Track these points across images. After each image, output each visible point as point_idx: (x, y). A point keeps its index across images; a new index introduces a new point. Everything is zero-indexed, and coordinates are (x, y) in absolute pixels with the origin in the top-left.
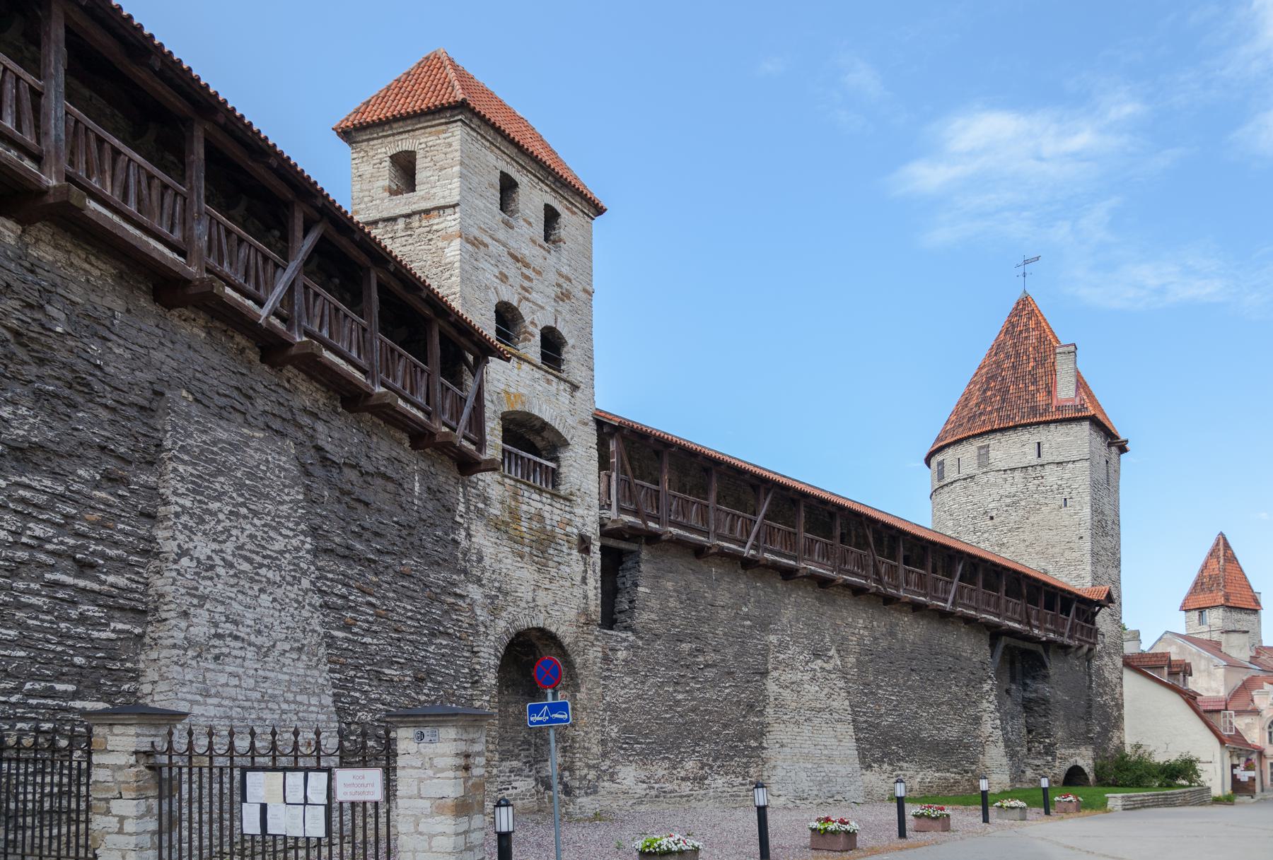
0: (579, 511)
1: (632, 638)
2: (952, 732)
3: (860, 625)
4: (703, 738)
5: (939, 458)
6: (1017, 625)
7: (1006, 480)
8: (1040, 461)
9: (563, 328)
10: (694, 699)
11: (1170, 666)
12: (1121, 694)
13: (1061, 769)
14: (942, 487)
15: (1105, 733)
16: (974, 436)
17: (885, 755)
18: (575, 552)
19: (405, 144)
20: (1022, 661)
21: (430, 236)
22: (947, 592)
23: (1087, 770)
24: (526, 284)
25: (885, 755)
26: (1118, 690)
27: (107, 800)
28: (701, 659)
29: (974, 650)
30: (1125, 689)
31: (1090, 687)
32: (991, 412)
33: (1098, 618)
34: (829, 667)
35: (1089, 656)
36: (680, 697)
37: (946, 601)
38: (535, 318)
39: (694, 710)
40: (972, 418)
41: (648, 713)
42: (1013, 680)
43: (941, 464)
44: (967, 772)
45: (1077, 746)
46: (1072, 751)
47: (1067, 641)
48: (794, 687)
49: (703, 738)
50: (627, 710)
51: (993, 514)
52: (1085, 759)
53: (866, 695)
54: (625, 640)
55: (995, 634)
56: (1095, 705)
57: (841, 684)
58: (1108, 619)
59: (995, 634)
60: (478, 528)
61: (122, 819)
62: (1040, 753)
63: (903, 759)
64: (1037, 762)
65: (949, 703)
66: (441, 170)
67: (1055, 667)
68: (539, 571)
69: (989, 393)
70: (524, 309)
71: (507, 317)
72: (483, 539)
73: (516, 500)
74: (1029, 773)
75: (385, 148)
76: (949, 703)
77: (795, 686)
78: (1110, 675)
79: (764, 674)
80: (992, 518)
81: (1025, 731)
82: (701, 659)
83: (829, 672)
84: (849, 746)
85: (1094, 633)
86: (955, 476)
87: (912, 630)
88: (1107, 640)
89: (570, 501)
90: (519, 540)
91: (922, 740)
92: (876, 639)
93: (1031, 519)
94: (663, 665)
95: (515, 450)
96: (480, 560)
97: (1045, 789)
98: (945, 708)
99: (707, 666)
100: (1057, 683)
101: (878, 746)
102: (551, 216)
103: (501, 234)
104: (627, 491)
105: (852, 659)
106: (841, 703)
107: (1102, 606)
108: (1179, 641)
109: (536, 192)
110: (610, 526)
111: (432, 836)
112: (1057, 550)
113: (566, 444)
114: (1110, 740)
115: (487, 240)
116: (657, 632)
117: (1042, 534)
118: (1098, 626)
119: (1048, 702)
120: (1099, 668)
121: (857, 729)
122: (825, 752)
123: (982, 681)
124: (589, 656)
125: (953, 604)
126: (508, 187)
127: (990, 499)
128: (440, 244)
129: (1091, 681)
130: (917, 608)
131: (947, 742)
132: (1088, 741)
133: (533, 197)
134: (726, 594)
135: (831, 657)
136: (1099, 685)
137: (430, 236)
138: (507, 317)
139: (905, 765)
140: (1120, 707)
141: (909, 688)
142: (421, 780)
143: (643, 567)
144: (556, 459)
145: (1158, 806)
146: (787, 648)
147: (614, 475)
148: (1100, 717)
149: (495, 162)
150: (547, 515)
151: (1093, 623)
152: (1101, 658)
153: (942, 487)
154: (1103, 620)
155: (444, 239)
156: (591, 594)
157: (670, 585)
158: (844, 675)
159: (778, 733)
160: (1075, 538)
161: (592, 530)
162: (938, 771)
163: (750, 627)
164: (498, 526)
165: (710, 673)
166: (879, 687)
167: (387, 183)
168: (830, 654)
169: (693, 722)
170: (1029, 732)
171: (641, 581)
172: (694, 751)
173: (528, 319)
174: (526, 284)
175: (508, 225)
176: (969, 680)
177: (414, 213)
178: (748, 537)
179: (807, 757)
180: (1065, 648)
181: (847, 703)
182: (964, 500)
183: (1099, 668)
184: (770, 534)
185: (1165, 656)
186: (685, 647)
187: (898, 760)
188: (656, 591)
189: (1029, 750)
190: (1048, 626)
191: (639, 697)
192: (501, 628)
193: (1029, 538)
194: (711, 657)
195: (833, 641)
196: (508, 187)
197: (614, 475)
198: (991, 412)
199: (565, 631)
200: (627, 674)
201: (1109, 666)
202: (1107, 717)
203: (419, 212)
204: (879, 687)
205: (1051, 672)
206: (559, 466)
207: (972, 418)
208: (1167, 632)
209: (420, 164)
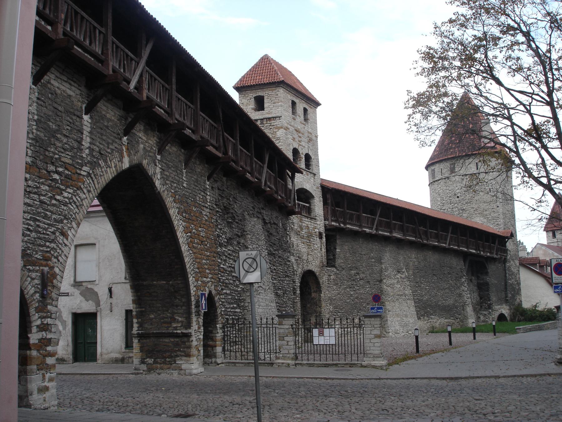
0: (318, 223)
1: (335, 270)
2: (450, 302)
3: (413, 257)
4: (360, 309)
5: (433, 168)
6: (474, 251)
7: (463, 179)
8: (477, 171)
9: (311, 154)
10: (357, 293)
11: (539, 263)
12: (519, 278)
13: (496, 315)
14: (434, 182)
15: (513, 297)
16: (448, 159)
17: (425, 313)
18: (318, 239)
19: (260, 93)
20: (477, 267)
21: (271, 127)
22: (446, 240)
23: (506, 315)
24: (300, 139)
25: (425, 313)
26: (518, 276)
27: (283, 337)
28: (358, 277)
29: (457, 264)
30: (521, 275)
31: (506, 276)
32: (455, 148)
33: (507, 244)
34: (403, 276)
35: (505, 261)
36: (352, 293)
37: (446, 243)
38: (303, 152)
39: (357, 298)
40: (446, 150)
41: (341, 300)
42: (473, 275)
43: (434, 170)
44: (457, 319)
45: (501, 304)
46: (499, 306)
47: (495, 256)
48: (391, 286)
49: (360, 309)
50: (335, 299)
51: (459, 195)
52: (505, 310)
53: (417, 287)
54: (333, 271)
55: (465, 256)
56: (508, 284)
57: (408, 283)
58: (512, 243)
59: (465, 256)
60: (292, 235)
61: (288, 342)
62: (486, 308)
63: (432, 314)
64: (485, 313)
65: (449, 288)
66: (274, 103)
67: (492, 268)
68: (308, 248)
69: (453, 139)
70: (300, 150)
71: (295, 152)
72: (294, 239)
73: (301, 222)
74: (482, 318)
75: (252, 95)
76: (449, 288)
77: (391, 286)
78: (515, 270)
79: (381, 281)
80: (458, 197)
81: (479, 298)
82: (358, 277)
83: (403, 278)
84: (413, 310)
85: (506, 251)
86: (440, 177)
87: (433, 257)
88: (512, 253)
89: (315, 219)
90: (302, 238)
91: (439, 305)
92: (419, 262)
93: (476, 198)
94: (346, 280)
95: (207, 118)
96: (293, 246)
97: (494, 326)
98: (447, 291)
99: (360, 279)
100: (493, 277)
101: (424, 309)
102: (305, 110)
103: (292, 124)
104: (334, 213)
105: (411, 272)
106: (408, 292)
107: (508, 239)
108: (544, 248)
109: (301, 104)
110: (328, 227)
111: (374, 343)
112: (488, 212)
113: (313, 197)
114: (516, 300)
115: (289, 127)
116: (343, 267)
117: (481, 205)
118: (507, 247)
119: (488, 284)
120: (509, 267)
121: (415, 302)
122: (404, 313)
123: (461, 277)
124: (324, 279)
125: (449, 245)
126: (294, 103)
127: (457, 188)
128: (275, 130)
129: (506, 273)
130: (435, 249)
131: (448, 306)
132: (506, 301)
133: (301, 105)
134: (366, 249)
135: (403, 272)
136: (509, 275)
137: (271, 127)
138: (295, 152)
139: (433, 317)
140: (519, 284)
141: (433, 283)
142: (371, 330)
143: (338, 242)
144: (309, 203)
145: (537, 330)
146: (388, 270)
147: (329, 207)
148: (510, 291)
149: (291, 97)
150: (309, 226)
151: (506, 247)
152: (510, 262)
153: (434, 182)
154: (509, 245)
155: (276, 128)
156: (323, 255)
157: (346, 247)
158: (408, 278)
159: (388, 306)
160: (495, 207)
161: (322, 230)
162: (446, 319)
163: (374, 262)
164: (298, 233)
165: (361, 282)
166: (421, 283)
167: (253, 107)
168: (403, 271)
169: (357, 303)
170: (481, 298)
171: (337, 247)
172: (358, 315)
173: (301, 152)
174: (300, 139)
175: (294, 119)
176: (456, 277)
177: (264, 119)
178: (373, 225)
179: (398, 315)
180: (494, 260)
181: (411, 291)
182: (445, 188)
183: (509, 267)
184: (380, 224)
185: (537, 258)
186: (353, 272)
187: (431, 315)
188: (342, 249)
189: (481, 307)
190: (487, 250)
191: (339, 294)
192: (300, 271)
193: (476, 206)
194: (362, 275)
195: (404, 265)
196: (294, 103)
197: (329, 207)
198: (455, 148)
199: (316, 270)
200: (334, 285)
201: (513, 265)
202: (514, 289)
203: (266, 118)
204: (421, 283)
205: (489, 271)
206: (310, 205)
207: (446, 150)
208: (538, 244)
209: (266, 101)
